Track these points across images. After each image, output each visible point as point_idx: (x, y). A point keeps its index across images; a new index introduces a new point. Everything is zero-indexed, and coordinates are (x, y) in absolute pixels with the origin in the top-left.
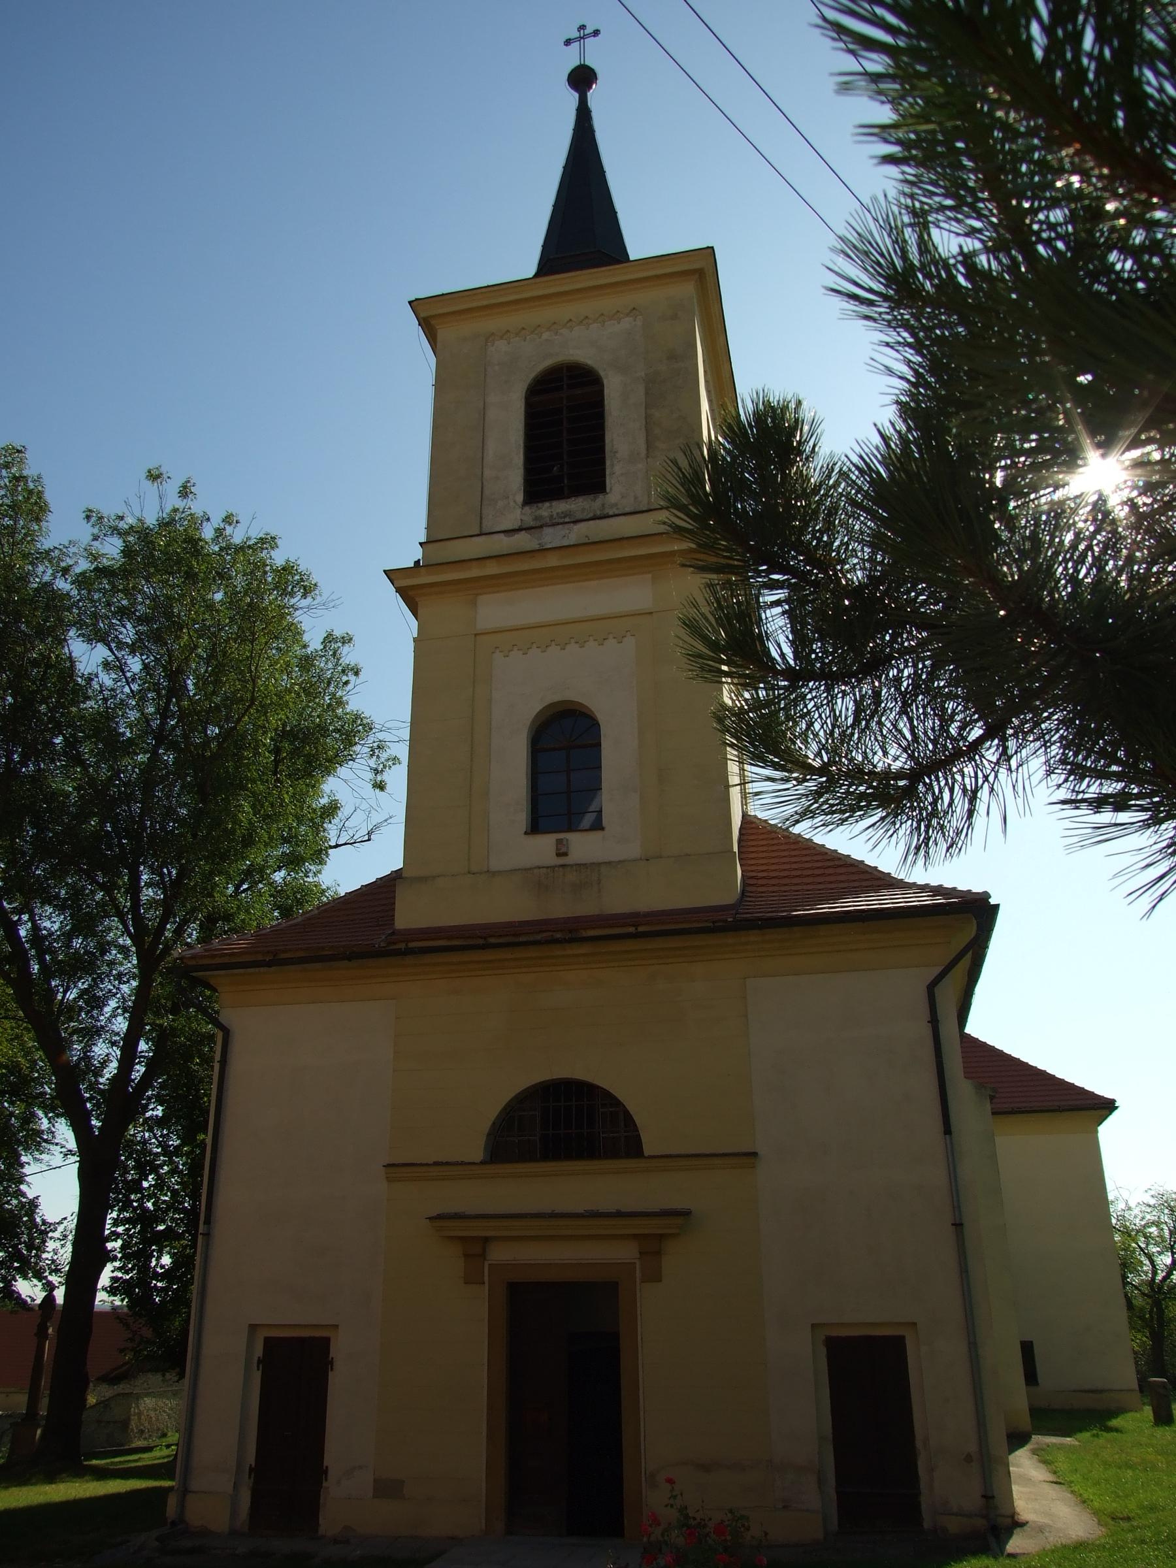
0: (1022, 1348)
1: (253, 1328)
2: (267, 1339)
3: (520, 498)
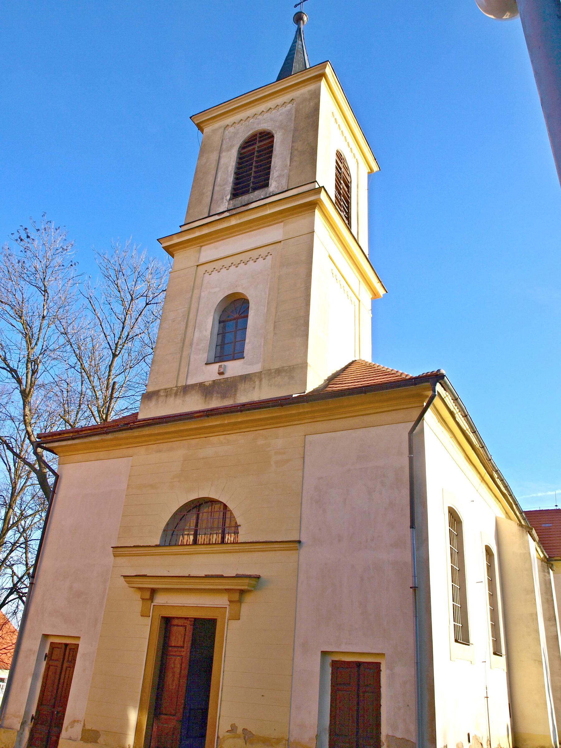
0: (210, 620)
1: (46, 636)
2: (52, 643)
3: (228, 197)
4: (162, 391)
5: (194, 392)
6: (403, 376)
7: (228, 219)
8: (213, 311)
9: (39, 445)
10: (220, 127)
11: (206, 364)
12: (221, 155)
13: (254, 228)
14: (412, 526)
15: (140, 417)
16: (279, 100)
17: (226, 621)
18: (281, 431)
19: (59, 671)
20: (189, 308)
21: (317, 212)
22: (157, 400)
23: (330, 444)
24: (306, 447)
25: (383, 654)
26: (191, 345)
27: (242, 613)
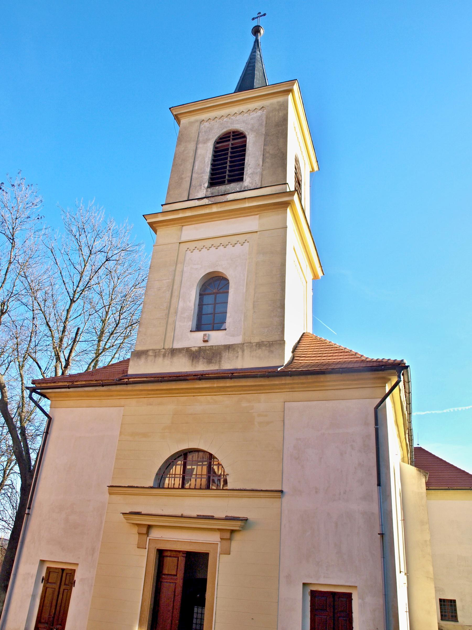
1: (42, 562)
3: (206, 185)
4: (151, 351)
5: (181, 355)
6: (363, 358)
7: (210, 206)
8: (196, 285)
9: (33, 390)
10: (197, 121)
11: (191, 331)
12: (198, 146)
13: (232, 217)
14: (379, 484)
15: (130, 372)
16: (251, 106)
17: (218, 555)
18: (263, 397)
19: (56, 593)
20: (174, 280)
21: (289, 210)
22: (146, 358)
23: (305, 410)
24: (285, 412)
25: (356, 587)
26: (176, 313)
27: (232, 549)
